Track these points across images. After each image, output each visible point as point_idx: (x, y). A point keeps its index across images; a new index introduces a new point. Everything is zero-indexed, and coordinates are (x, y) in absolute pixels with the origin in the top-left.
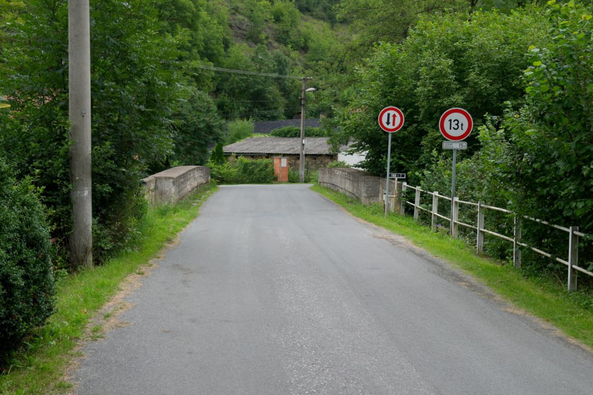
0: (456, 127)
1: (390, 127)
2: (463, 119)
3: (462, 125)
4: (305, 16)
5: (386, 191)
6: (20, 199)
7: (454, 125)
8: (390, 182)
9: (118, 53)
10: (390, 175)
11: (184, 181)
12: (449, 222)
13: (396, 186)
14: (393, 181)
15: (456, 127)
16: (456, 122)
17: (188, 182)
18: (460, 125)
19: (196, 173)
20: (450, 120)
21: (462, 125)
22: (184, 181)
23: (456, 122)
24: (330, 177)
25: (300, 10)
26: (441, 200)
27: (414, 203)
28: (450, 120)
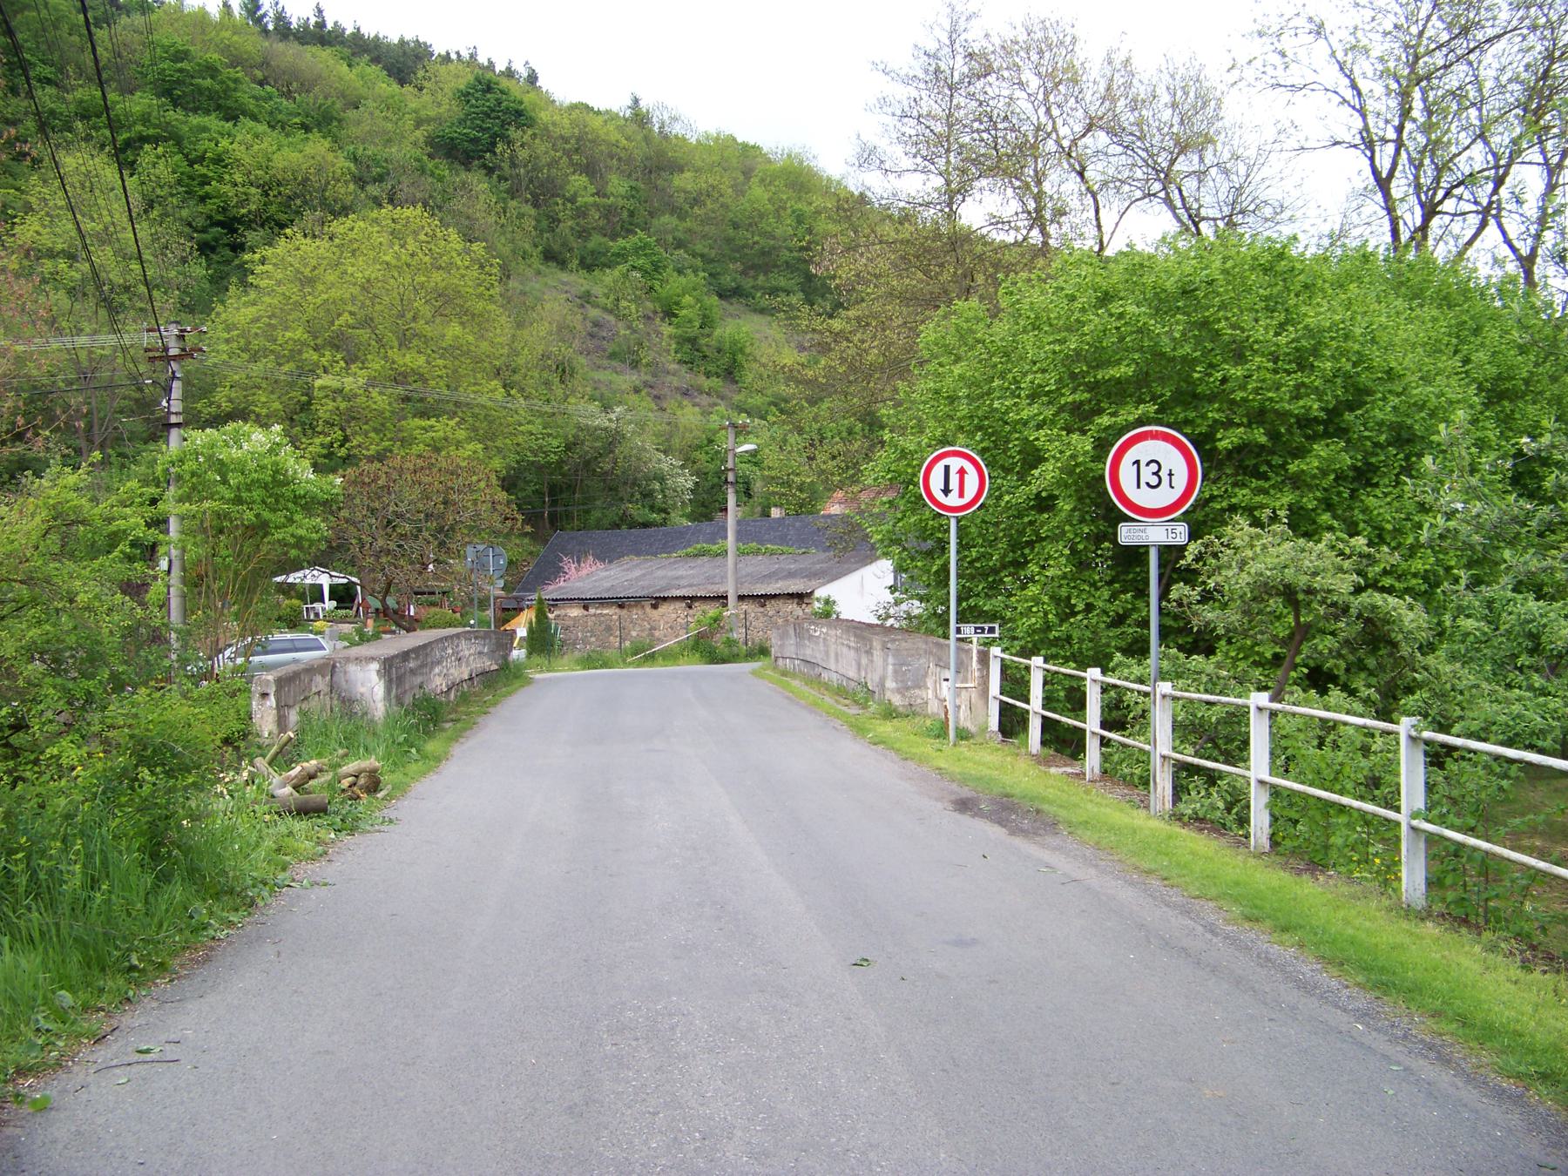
0: (1154, 481)
1: (953, 500)
2: (1173, 460)
3: (1170, 475)
4: (731, 309)
5: (949, 674)
6: (1331, 529)
7: (1147, 474)
8: (958, 649)
9: (1528, 907)
10: (958, 631)
11: (422, 666)
12: (1147, 753)
13: (975, 658)
14: (966, 646)
15: (1154, 481)
16: (1154, 467)
17: (437, 670)
18: (1164, 474)
19: (463, 644)
20: (1137, 462)
21: (1170, 475)
22: (422, 666)
23: (1154, 467)
24: (797, 645)
25: (720, 296)
26: (1105, 689)
27: (1027, 702)
28: (1137, 462)
